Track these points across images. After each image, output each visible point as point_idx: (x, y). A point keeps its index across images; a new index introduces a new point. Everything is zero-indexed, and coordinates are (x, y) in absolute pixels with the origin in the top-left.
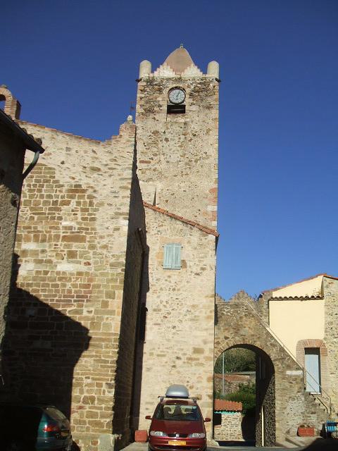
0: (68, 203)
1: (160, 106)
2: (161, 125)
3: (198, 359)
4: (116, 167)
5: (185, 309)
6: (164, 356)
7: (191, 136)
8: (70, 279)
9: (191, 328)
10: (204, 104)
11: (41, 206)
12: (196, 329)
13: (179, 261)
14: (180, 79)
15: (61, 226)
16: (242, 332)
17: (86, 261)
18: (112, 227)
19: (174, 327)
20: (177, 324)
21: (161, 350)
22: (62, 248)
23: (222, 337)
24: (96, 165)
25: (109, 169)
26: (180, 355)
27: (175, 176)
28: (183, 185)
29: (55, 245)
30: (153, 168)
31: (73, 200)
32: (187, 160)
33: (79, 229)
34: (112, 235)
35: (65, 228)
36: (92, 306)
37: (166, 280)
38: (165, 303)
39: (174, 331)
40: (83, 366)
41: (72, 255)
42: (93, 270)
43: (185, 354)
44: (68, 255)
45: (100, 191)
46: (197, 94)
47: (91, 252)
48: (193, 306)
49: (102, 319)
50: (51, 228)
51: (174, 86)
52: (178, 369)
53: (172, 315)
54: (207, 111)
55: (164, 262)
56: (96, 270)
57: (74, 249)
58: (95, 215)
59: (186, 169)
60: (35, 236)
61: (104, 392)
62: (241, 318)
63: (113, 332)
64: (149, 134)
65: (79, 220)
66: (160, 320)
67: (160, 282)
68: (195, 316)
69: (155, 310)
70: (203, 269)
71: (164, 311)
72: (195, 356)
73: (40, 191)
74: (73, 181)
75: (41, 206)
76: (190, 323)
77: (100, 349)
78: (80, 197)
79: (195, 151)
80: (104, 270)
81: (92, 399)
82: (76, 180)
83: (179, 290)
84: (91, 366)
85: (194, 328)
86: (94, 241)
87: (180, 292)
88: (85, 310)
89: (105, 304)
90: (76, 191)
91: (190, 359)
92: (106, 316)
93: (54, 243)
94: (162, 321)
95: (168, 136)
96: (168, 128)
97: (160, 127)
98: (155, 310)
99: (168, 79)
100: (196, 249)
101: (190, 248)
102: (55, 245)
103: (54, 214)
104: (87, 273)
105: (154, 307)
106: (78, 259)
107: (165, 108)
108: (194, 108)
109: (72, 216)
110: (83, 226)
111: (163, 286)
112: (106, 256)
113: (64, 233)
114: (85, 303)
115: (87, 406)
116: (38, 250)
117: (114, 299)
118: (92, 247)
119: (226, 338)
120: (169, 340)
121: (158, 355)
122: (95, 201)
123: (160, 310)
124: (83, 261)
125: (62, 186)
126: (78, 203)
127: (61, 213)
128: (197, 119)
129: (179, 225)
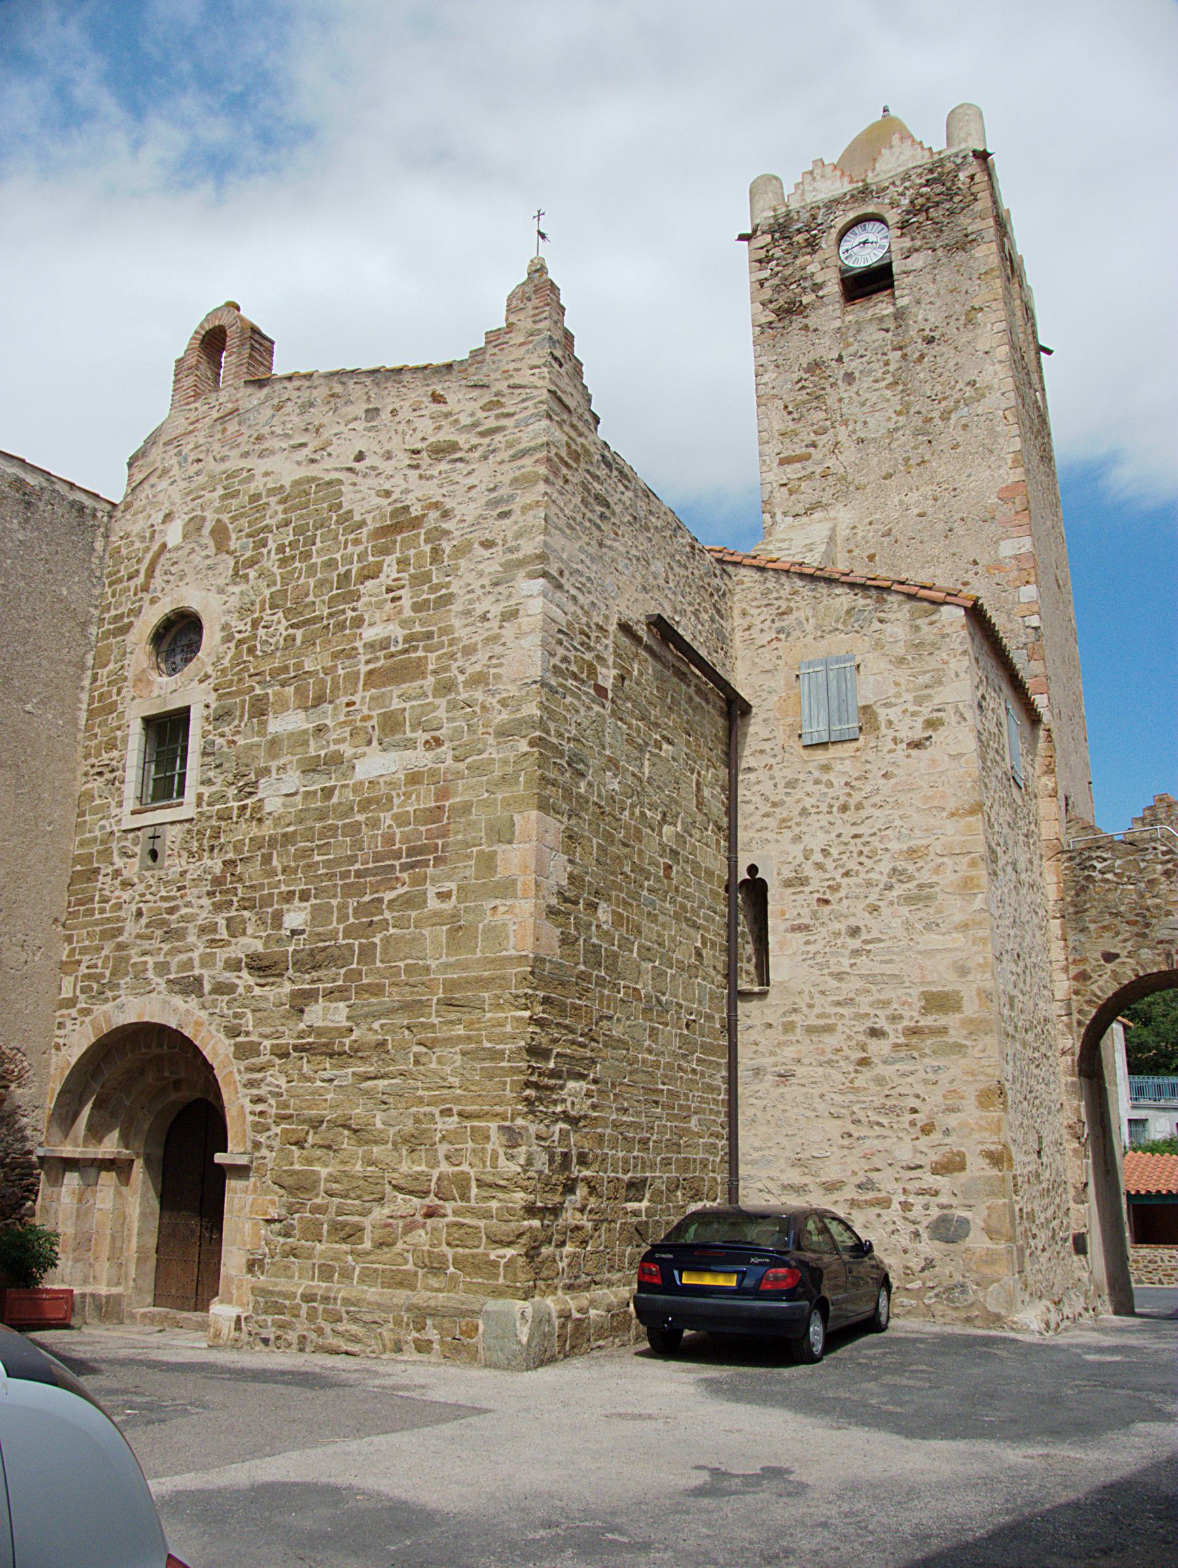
0: (370, 573)
1: (817, 287)
2: (826, 341)
3: (944, 1030)
4: (504, 422)
5: (885, 866)
6: (829, 1029)
7: (920, 345)
8: (390, 799)
9: (908, 926)
10: (948, 237)
11: (311, 598)
12: (927, 927)
13: (853, 712)
14: (864, 193)
15: (359, 644)
16: (1159, 932)
17: (427, 736)
18: (496, 611)
19: (854, 932)
20: (862, 918)
21: (817, 1010)
22: (366, 712)
23: (1095, 956)
24: (447, 435)
25: (482, 434)
26: (882, 1023)
27: (888, 476)
28: (914, 497)
29: (348, 705)
30: (819, 470)
31: (388, 559)
32: (918, 421)
33: (407, 640)
34: (495, 638)
35: (370, 646)
36: (449, 878)
37: (817, 782)
38: (818, 857)
39: (855, 943)
40: (434, 1072)
41: (391, 723)
42: (449, 761)
43: (894, 1018)
44: (383, 728)
45: (459, 511)
46: (921, 217)
47: (442, 702)
48: (912, 853)
49: (478, 911)
50: (335, 656)
51: (851, 215)
52: (880, 1069)
53: (842, 894)
54: (960, 256)
55: (805, 724)
56: (457, 759)
57: (396, 704)
58: (447, 585)
59: (915, 448)
60: (297, 689)
61: (495, 1156)
62: (1151, 882)
63: (513, 952)
64: (795, 377)
65: (408, 613)
66: (805, 911)
67: (798, 793)
68: (920, 886)
69: (788, 884)
70: (931, 724)
71: (817, 882)
72: (927, 1021)
73: (307, 556)
74: (385, 502)
75: (311, 598)
76: (904, 910)
77: (477, 1013)
78: (407, 544)
79: (939, 388)
80: (481, 752)
81: (462, 1183)
82: (394, 497)
83: (859, 807)
84: (454, 1073)
85: (919, 926)
86: (447, 669)
87: (863, 813)
88: (432, 891)
89: (488, 862)
90: (396, 528)
91: (914, 1032)
92: (489, 904)
93: (345, 700)
94: (814, 914)
95: (852, 365)
96: (848, 345)
97: (826, 350)
98: (788, 884)
99: (832, 205)
100: (902, 660)
101: (883, 664)
102: (348, 705)
103: (343, 611)
104: (433, 773)
105: (788, 874)
106: (409, 735)
107: (833, 288)
108: (918, 261)
109: (389, 606)
110: (418, 629)
111: (808, 802)
112: (483, 707)
113: (368, 662)
114: (430, 871)
115: (449, 1207)
116: (305, 732)
117: (510, 842)
118: (447, 687)
119: (1109, 957)
120: (839, 976)
121: (811, 1030)
122: (446, 546)
123: (803, 881)
124: (422, 736)
125: (363, 524)
126: (403, 563)
127: (359, 605)
128: (932, 289)
129: (844, 599)
